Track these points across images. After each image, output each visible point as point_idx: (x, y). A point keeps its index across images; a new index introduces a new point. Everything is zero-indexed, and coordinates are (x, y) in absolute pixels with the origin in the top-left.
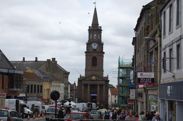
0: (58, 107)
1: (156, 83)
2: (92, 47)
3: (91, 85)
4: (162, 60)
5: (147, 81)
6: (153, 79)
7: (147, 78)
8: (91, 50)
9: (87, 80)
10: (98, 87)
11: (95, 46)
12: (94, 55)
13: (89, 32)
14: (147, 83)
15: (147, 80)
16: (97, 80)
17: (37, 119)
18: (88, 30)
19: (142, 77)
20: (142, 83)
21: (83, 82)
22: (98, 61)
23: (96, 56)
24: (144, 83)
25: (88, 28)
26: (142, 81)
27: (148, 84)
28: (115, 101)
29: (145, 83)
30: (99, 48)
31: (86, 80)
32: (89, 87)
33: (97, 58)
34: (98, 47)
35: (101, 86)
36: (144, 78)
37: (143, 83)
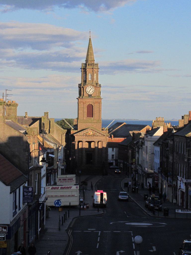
7: (190, 183)
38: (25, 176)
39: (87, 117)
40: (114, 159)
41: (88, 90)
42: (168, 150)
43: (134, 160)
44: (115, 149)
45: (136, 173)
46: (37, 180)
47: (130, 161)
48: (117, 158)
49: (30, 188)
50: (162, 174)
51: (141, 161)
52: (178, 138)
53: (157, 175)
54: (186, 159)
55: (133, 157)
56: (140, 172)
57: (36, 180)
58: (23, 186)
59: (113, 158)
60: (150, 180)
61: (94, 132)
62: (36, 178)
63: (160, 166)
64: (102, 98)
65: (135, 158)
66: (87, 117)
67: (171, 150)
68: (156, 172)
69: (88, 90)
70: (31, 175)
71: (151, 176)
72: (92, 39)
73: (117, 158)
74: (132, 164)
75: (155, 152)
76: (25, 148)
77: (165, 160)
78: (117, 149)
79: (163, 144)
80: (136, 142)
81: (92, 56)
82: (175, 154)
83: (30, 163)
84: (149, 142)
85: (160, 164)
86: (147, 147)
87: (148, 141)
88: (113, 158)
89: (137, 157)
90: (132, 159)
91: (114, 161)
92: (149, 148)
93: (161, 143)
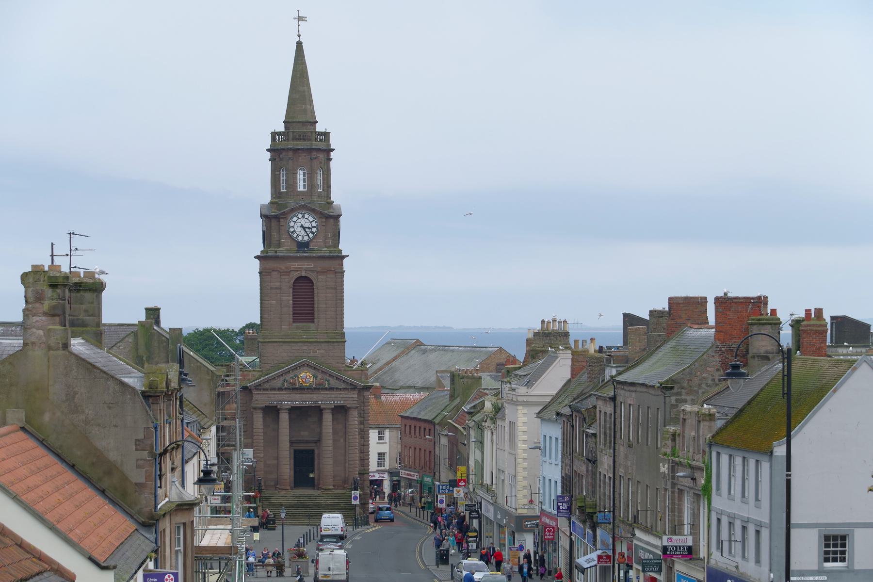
1: (696, 555)
3: (292, 410)
5: (680, 551)
6: (690, 549)
7: (680, 546)
8: (284, 250)
9: (274, 389)
10: (328, 417)
12: (304, 268)
13: (272, 160)
14: (680, 554)
15: (680, 548)
16: (318, 388)
17: (252, 580)
19: (671, 544)
20: (671, 554)
21: (257, 395)
22: (321, 297)
23: (312, 276)
24: (674, 555)
25: (268, 144)
26: (671, 551)
27: (682, 557)
28: (381, 455)
29: (677, 555)
30: (321, 238)
31: (272, 389)
32: (284, 417)
33: (314, 282)
34: (317, 231)
35: (341, 411)
36: (675, 546)
37: (673, 554)
38: (146, 535)
39: (295, 321)
40: (387, 467)
41: (295, 227)
42: (594, 435)
43: (462, 469)
44: (387, 433)
45: (474, 514)
46: (181, 548)
47: (445, 475)
48: (397, 466)
49: (169, 576)
50: (573, 519)
51: (492, 473)
52: (632, 391)
53: (553, 524)
54: (666, 466)
55: (457, 458)
56: (488, 511)
57: (177, 549)
58: (144, 570)
59: (381, 463)
60: (528, 542)
61: (320, 376)
62: (179, 539)
63: (563, 487)
64: (344, 254)
65: (465, 461)
66: (295, 321)
67: (605, 434)
68: (550, 510)
69: (293, 227)
70: (164, 530)
71: (529, 524)
72: (305, 46)
73: (397, 466)
74: (454, 483)
75: (542, 443)
76: (141, 436)
77: (581, 467)
78: (397, 434)
79: (574, 414)
80: (468, 407)
81: (308, 106)
82: (622, 450)
83: (161, 487)
84: (520, 408)
85: (563, 483)
86: (513, 424)
87: (516, 403)
88: (384, 466)
89: (476, 461)
90: (453, 466)
91: (386, 476)
92: (521, 428)
93: (567, 411)
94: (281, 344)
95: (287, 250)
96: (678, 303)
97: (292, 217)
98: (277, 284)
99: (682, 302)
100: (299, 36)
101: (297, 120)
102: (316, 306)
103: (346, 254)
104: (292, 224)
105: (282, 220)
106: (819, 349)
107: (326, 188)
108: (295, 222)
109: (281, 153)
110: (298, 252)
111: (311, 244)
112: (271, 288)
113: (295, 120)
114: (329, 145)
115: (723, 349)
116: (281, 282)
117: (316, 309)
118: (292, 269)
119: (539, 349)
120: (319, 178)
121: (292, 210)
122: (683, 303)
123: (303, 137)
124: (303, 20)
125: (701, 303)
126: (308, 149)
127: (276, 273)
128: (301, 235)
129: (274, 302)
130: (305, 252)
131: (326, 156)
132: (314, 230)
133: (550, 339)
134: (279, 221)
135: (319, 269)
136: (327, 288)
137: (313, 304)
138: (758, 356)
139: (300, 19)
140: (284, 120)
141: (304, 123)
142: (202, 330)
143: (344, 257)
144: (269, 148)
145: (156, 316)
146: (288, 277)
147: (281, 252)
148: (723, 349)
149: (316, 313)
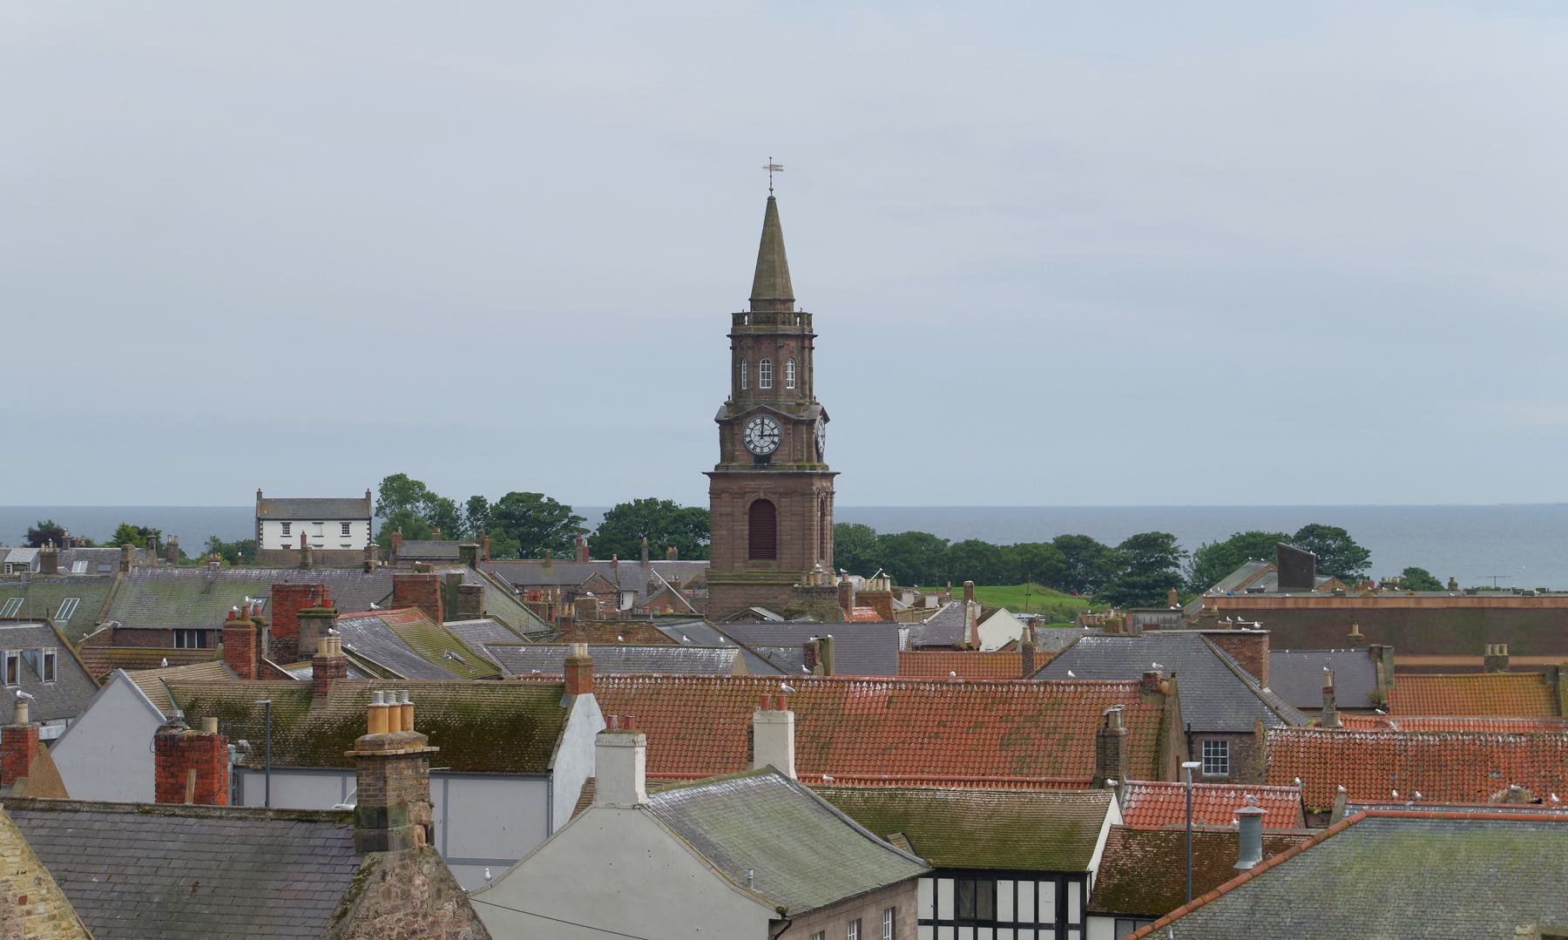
0: (1492, 653)
2: (745, 445)
4: (297, 528)
8: (741, 464)
11: (761, 436)
12: (762, 489)
18: (813, 348)
22: (786, 525)
23: (774, 499)
33: (776, 507)
34: (781, 440)
39: (752, 557)
41: (753, 435)
64: (831, 470)
66: (752, 557)
94: (732, 587)
95: (742, 467)
96: (403, 582)
97: (749, 423)
98: (729, 509)
99: (408, 580)
100: (771, 190)
101: (763, 298)
102: (778, 537)
103: (836, 471)
104: (748, 432)
105: (736, 427)
106: (241, 654)
107: (799, 385)
108: (752, 429)
109: (741, 341)
110: (755, 467)
111: (773, 458)
112: (721, 515)
113: (760, 298)
114: (811, 331)
115: (279, 646)
116: (733, 507)
117: (778, 542)
118: (748, 490)
119: (796, 608)
120: (790, 372)
121: (749, 414)
122: (409, 582)
123: (771, 320)
124: (777, 170)
125: (430, 581)
126: (771, 335)
127: (727, 495)
128: (764, 446)
129: (725, 532)
130: (763, 468)
131: (800, 344)
132: (776, 439)
133: (811, 596)
134: (733, 429)
135: (781, 490)
136: (792, 515)
137: (775, 536)
138: (306, 655)
139: (772, 168)
140: (750, 297)
141: (772, 302)
142: (1244, 534)
143: (834, 474)
144: (730, 333)
145: (472, 556)
146: (741, 500)
147: (734, 467)
148: (279, 646)
149: (778, 547)
